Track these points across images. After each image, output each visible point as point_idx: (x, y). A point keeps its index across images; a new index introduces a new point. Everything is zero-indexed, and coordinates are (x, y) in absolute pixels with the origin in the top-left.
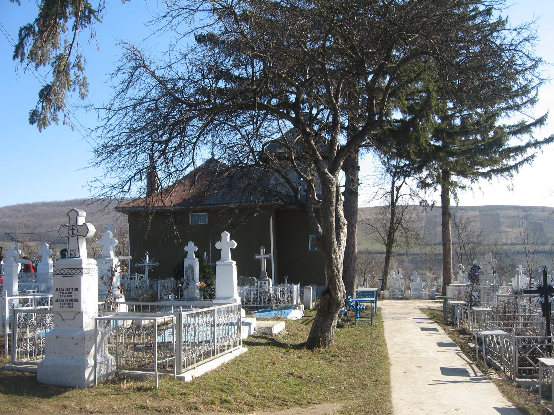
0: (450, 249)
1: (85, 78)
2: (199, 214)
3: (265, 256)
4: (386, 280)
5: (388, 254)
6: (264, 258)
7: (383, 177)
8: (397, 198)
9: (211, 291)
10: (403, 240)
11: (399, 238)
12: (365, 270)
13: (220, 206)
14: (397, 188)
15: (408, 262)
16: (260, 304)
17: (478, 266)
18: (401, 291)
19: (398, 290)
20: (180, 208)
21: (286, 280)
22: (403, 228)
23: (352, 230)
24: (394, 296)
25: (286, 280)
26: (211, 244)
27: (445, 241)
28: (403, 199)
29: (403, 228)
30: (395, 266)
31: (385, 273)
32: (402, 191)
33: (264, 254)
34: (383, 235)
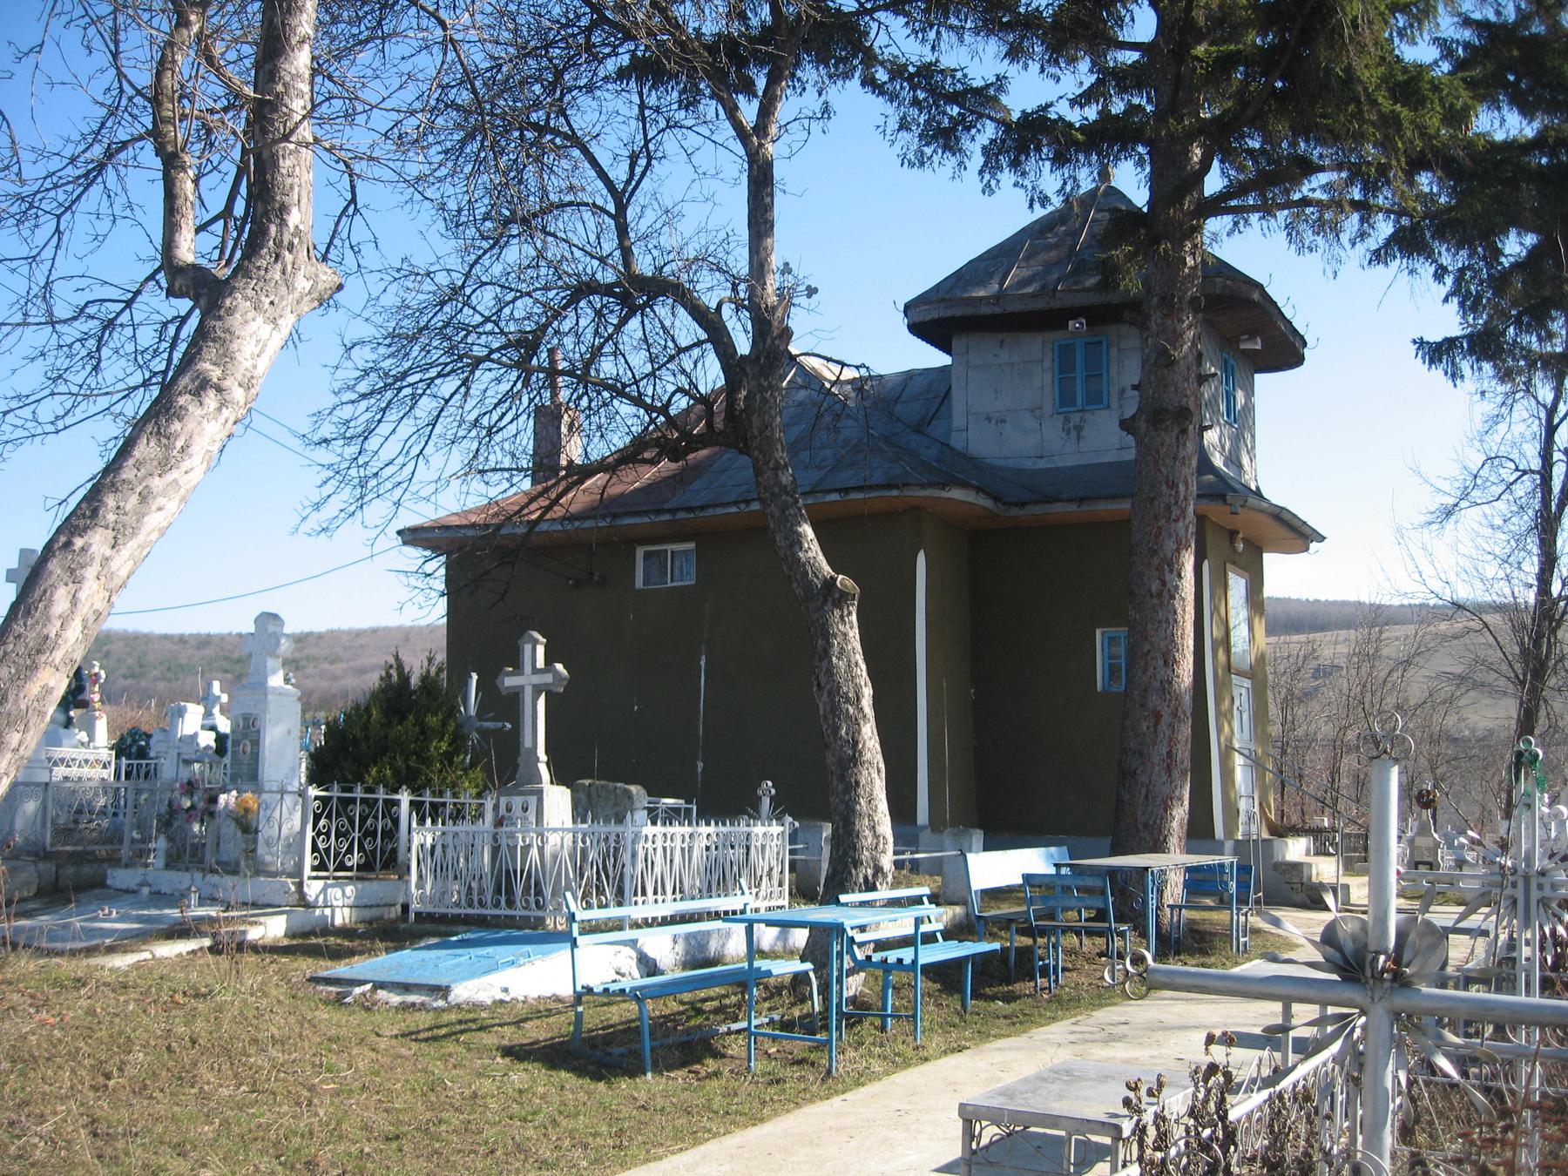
2: (670, 547)
3: (537, 679)
6: (537, 690)
9: (838, 850)
21: (766, 801)
23: (1164, 583)
25: (766, 801)
26: (703, 663)
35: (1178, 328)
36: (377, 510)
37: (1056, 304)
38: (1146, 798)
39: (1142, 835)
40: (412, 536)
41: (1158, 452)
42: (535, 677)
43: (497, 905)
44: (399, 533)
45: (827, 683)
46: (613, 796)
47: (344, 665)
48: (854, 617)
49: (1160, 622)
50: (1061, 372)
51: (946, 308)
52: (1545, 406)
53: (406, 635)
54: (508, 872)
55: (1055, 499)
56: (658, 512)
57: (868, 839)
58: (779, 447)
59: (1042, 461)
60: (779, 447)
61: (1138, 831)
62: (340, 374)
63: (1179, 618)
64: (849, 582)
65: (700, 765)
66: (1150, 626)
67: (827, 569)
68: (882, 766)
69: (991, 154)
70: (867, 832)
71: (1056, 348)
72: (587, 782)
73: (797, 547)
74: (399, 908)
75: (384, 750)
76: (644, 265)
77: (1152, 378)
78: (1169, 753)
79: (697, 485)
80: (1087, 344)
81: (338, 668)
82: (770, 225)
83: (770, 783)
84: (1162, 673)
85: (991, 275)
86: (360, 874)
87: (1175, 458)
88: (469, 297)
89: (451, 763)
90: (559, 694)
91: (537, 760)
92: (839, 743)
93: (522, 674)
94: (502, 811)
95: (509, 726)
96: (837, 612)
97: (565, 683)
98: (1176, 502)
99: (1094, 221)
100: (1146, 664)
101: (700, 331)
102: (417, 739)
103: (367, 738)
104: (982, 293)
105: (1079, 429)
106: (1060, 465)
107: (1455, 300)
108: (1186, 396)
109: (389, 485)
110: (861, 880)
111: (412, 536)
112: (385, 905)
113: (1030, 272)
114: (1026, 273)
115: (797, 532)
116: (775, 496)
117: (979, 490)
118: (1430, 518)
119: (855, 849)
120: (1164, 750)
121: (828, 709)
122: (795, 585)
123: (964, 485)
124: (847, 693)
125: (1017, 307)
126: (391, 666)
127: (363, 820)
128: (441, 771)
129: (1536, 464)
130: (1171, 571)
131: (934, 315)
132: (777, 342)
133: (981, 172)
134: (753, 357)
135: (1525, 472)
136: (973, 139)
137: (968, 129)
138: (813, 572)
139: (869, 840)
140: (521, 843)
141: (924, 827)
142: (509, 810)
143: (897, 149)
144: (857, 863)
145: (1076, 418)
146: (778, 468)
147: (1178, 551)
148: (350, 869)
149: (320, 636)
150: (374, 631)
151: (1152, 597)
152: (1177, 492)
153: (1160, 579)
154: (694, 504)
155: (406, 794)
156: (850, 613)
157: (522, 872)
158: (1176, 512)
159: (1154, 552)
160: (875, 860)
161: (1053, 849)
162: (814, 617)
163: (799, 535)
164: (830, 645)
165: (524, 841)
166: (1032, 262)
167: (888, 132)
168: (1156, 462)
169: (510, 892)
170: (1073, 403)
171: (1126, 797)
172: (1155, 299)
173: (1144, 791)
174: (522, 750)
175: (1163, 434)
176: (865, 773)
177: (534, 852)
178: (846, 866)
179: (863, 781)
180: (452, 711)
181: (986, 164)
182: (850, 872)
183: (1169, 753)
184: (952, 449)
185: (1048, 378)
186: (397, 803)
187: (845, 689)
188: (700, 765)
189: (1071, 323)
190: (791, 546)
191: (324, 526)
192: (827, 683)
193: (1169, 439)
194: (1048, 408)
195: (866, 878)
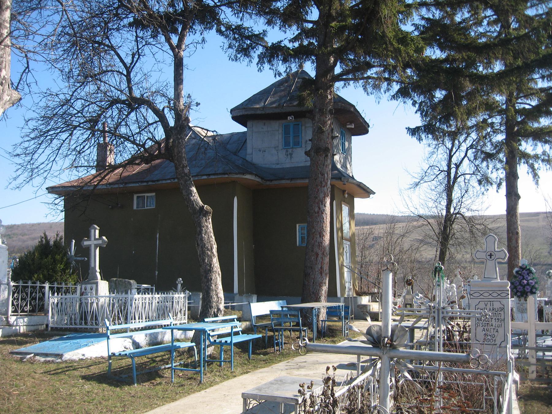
0: (518, 246)
1: (420, 139)
2: (146, 195)
3: (96, 242)
8: (456, 178)
13: (164, 182)
14: (456, 164)
16: (81, 324)
17: (529, 269)
21: (179, 286)
23: (320, 209)
25: (179, 286)
26: (158, 236)
27: (511, 235)
36: (38, 180)
38: (313, 283)
39: (312, 296)
40: (51, 190)
41: (318, 163)
43: (81, 324)
44: (47, 189)
45: (201, 243)
47: (27, 237)
48: (210, 220)
49: (318, 222)
52: (448, 149)
53: (51, 226)
54: (85, 312)
55: (282, 179)
56: (142, 182)
57: (215, 299)
58: (184, 159)
60: (184, 159)
61: (310, 295)
63: (325, 221)
64: (209, 208)
65: (157, 272)
66: (315, 223)
67: (201, 203)
68: (220, 273)
69: (261, 58)
71: (283, 126)
72: (115, 279)
73: (190, 195)
74: (45, 326)
76: (137, 93)
79: (156, 172)
81: (25, 238)
83: (181, 279)
84: (318, 240)
88: (72, 104)
91: (96, 271)
92: (205, 264)
93: (90, 240)
96: (204, 218)
97: (106, 243)
100: (313, 237)
102: (52, 264)
104: (258, 106)
105: (291, 154)
106: (284, 167)
107: (419, 112)
108: (328, 144)
109: (42, 171)
111: (51, 190)
114: (273, 100)
117: (256, 175)
118: (411, 186)
119: (210, 302)
120: (320, 267)
121: (201, 253)
122: (189, 209)
123: (251, 173)
125: (271, 111)
127: (31, 293)
128: (61, 275)
129: (446, 168)
130: (322, 204)
131: (241, 114)
133: (257, 64)
136: (255, 52)
137: (253, 49)
138: (196, 204)
140: (90, 302)
141: (237, 294)
142: (85, 289)
145: (290, 151)
148: (26, 312)
149: (18, 226)
150: (39, 224)
154: (155, 179)
155: (47, 284)
156: (209, 219)
157: (90, 312)
160: (218, 306)
161: (281, 301)
162: (196, 220)
163: (191, 191)
164: (202, 230)
165: (91, 301)
166: (275, 96)
167: (224, 49)
168: (317, 166)
169: (86, 319)
171: (306, 283)
172: (317, 110)
173: (312, 281)
174: (90, 268)
177: (95, 305)
178: (207, 308)
179: (213, 278)
180: (66, 254)
181: (259, 61)
183: (321, 268)
185: (280, 136)
186: (44, 287)
188: (157, 272)
190: (188, 195)
192: (201, 243)
193: (322, 158)
194: (280, 147)
195: (214, 312)
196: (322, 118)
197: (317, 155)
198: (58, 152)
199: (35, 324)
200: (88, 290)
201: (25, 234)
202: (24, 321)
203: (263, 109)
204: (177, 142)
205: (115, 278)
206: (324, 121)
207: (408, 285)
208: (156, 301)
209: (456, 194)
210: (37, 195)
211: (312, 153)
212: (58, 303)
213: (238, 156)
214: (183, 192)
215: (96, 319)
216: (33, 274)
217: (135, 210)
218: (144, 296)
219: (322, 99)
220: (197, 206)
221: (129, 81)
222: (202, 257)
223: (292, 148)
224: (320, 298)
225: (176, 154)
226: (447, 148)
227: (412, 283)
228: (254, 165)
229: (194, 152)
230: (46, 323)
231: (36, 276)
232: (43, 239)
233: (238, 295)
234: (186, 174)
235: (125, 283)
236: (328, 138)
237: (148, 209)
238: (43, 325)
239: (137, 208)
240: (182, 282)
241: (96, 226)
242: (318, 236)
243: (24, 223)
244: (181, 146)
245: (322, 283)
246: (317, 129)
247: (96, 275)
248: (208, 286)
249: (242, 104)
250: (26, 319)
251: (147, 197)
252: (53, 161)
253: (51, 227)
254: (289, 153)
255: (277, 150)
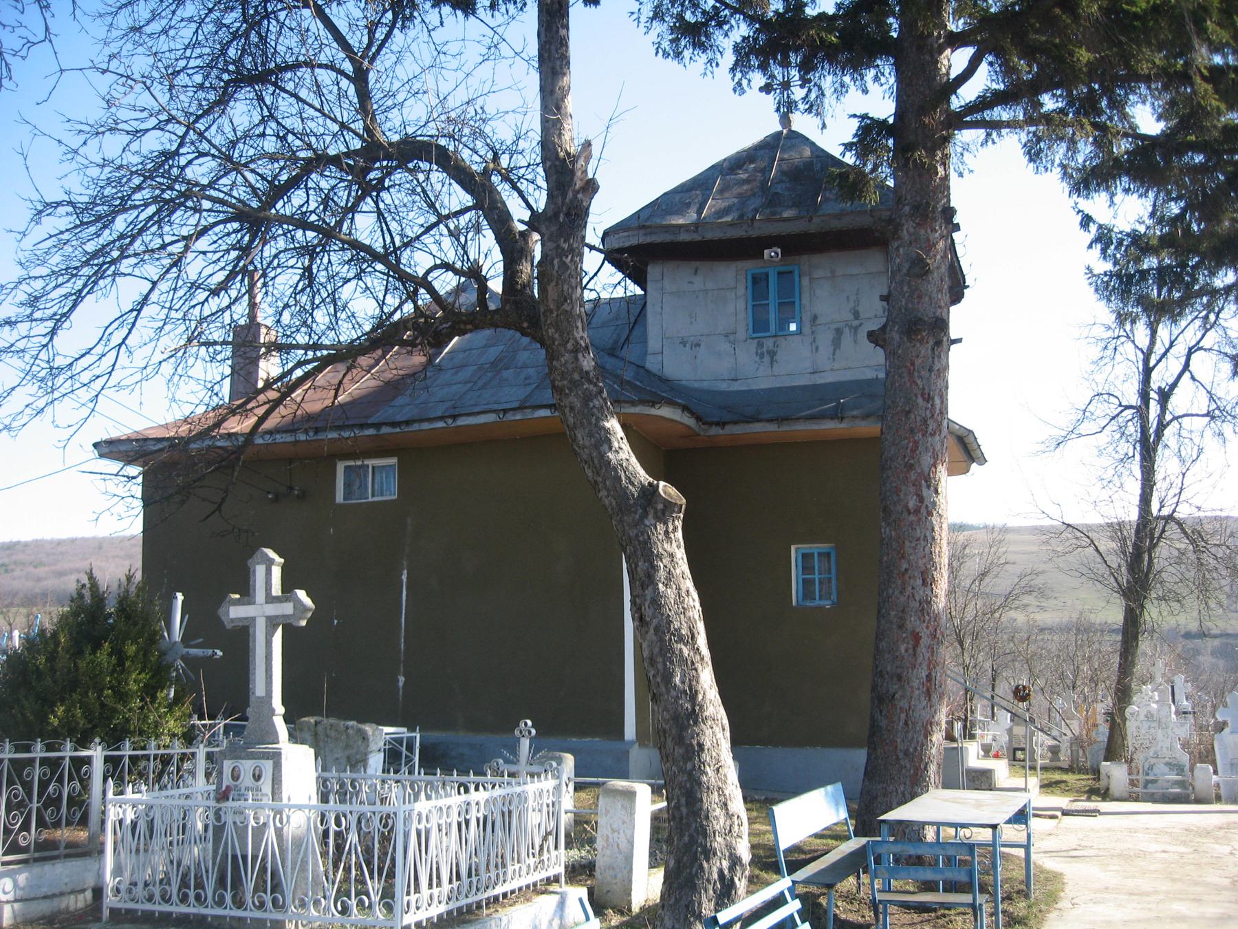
2: (371, 462)
3: (273, 610)
4: (1124, 720)
5: (1132, 629)
6: (272, 623)
7: (1109, 352)
8: (1162, 426)
10: (1187, 575)
11: (1170, 569)
12: (1076, 677)
15: (1212, 654)
18: (1179, 769)
19: (1167, 764)
20: (288, 438)
21: (525, 744)
22: (1185, 533)
23: (921, 500)
24: (1152, 789)
25: (525, 744)
26: (404, 578)
28: (1184, 433)
29: (1185, 533)
30: (1160, 667)
31: (1123, 695)
32: (1178, 403)
33: (270, 599)
34: (1114, 561)
35: (931, 238)
36: (67, 411)
37: (754, 233)
38: (906, 723)
39: (902, 762)
40: (109, 448)
41: (913, 364)
42: (270, 606)
43: (220, 902)
44: (96, 445)
45: (654, 617)
46: (344, 737)
47: (47, 569)
48: (679, 534)
49: (918, 539)
50: (754, 299)
51: (646, 235)
52: (1141, 350)
53: (99, 546)
54: (235, 857)
55: (755, 419)
56: (362, 426)
57: (718, 821)
58: (579, 324)
59: (736, 384)
60: (579, 324)
61: (898, 759)
62: (28, 243)
63: (937, 536)
64: (673, 491)
65: (402, 679)
66: (907, 543)
67: (643, 476)
68: (726, 722)
69: (745, 55)
70: (718, 810)
71: (750, 278)
72: (312, 720)
73: (606, 447)
74: (89, 895)
75: (73, 685)
76: (391, 129)
77: (905, 289)
78: (929, 677)
79: (400, 401)
80: (780, 273)
81: (41, 571)
82: (565, 60)
83: (529, 723)
84: (920, 593)
85: (688, 205)
86: (37, 855)
87: (930, 370)
88: (183, 168)
89: (154, 698)
90: (302, 627)
91: (273, 712)
92: (673, 693)
93: (252, 602)
94: (227, 781)
95: (220, 653)
96: (660, 528)
97: (310, 614)
98: (933, 416)
99: (781, 160)
100: (904, 583)
101: (469, 197)
102: (114, 671)
103: (53, 670)
104: (681, 221)
105: (772, 354)
106: (754, 387)
107: (1099, 246)
108: (940, 307)
109: (85, 377)
110: (715, 876)
111: (109, 448)
112: (72, 892)
113: (727, 204)
114: (722, 204)
115: (604, 428)
116: (575, 384)
117: (685, 408)
118: (1042, 447)
119: (705, 835)
120: (924, 674)
121: (656, 650)
122: (603, 493)
123: (671, 403)
124: (680, 629)
125: (715, 235)
126: (84, 586)
127: (43, 785)
128: (142, 708)
129: (1134, 400)
130: (929, 487)
131: (634, 241)
132: (580, 196)
133: (733, 70)
134: (550, 213)
135: (1127, 407)
136: (726, 35)
137: (720, 25)
138: (627, 478)
139: (722, 821)
140: (252, 823)
141: (631, 743)
142: (235, 776)
143: (653, 36)
144: (708, 853)
145: (769, 343)
146: (577, 350)
147: (935, 466)
148: (24, 850)
149: (26, 545)
150: (73, 541)
151: (909, 513)
152: (932, 405)
153: (918, 495)
154: (399, 418)
155: (99, 748)
156: (675, 529)
157: (255, 858)
158: (932, 425)
159: (911, 467)
160: (730, 847)
161: (829, 788)
162: (633, 533)
163: (607, 431)
164: (655, 569)
165: (256, 818)
166: (727, 195)
167: (643, 19)
168: (911, 374)
169: (237, 883)
170: (767, 329)
171: (884, 723)
172: (907, 208)
173: (903, 716)
174: (252, 699)
175: (918, 345)
176: (708, 732)
177: (271, 833)
178: (695, 858)
179: (708, 744)
180: (153, 638)
181: (736, 64)
182: (701, 865)
183: (929, 677)
184: (647, 371)
185: (741, 305)
186: (88, 761)
187: (677, 625)
188: (402, 679)
189: (766, 251)
190: (597, 446)
191: (7, 422)
192: (654, 617)
193: (925, 350)
194: (742, 334)
195: (721, 872)
196: (922, 232)
197: (910, 340)
198: (136, 318)
199: (56, 891)
200: (246, 780)
201: (41, 564)
202: (16, 885)
203: (697, 228)
204: (556, 262)
205: (312, 715)
206: (928, 240)
207: (1019, 701)
208: (481, 815)
209: (1166, 464)
210: (75, 388)
211: (895, 335)
212: (134, 825)
213: (622, 359)
214: (579, 436)
215: (276, 887)
216: (53, 704)
217: (341, 505)
218: (443, 802)
219: (920, 176)
220: (633, 484)
221: (364, 94)
222: (660, 666)
223: (775, 336)
224: (926, 768)
225: (552, 306)
226: (1137, 347)
227: (1028, 695)
228: (665, 381)
229: (501, 348)
230: (91, 882)
231: (60, 710)
232: (84, 591)
233: (636, 745)
234: (587, 373)
235: (348, 736)
236: (940, 291)
237: (373, 502)
238: (83, 891)
239: (345, 499)
240: (533, 731)
241: (271, 554)
242: (919, 582)
243: (39, 537)
244: (570, 276)
245: (931, 724)
246: (906, 266)
247: (273, 725)
248: (690, 774)
249: (637, 215)
250: (22, 878)
251: (373, 468)
252: (120, 345)
253: (100, 548)
254: (765, 349)
255: (733, 343)
